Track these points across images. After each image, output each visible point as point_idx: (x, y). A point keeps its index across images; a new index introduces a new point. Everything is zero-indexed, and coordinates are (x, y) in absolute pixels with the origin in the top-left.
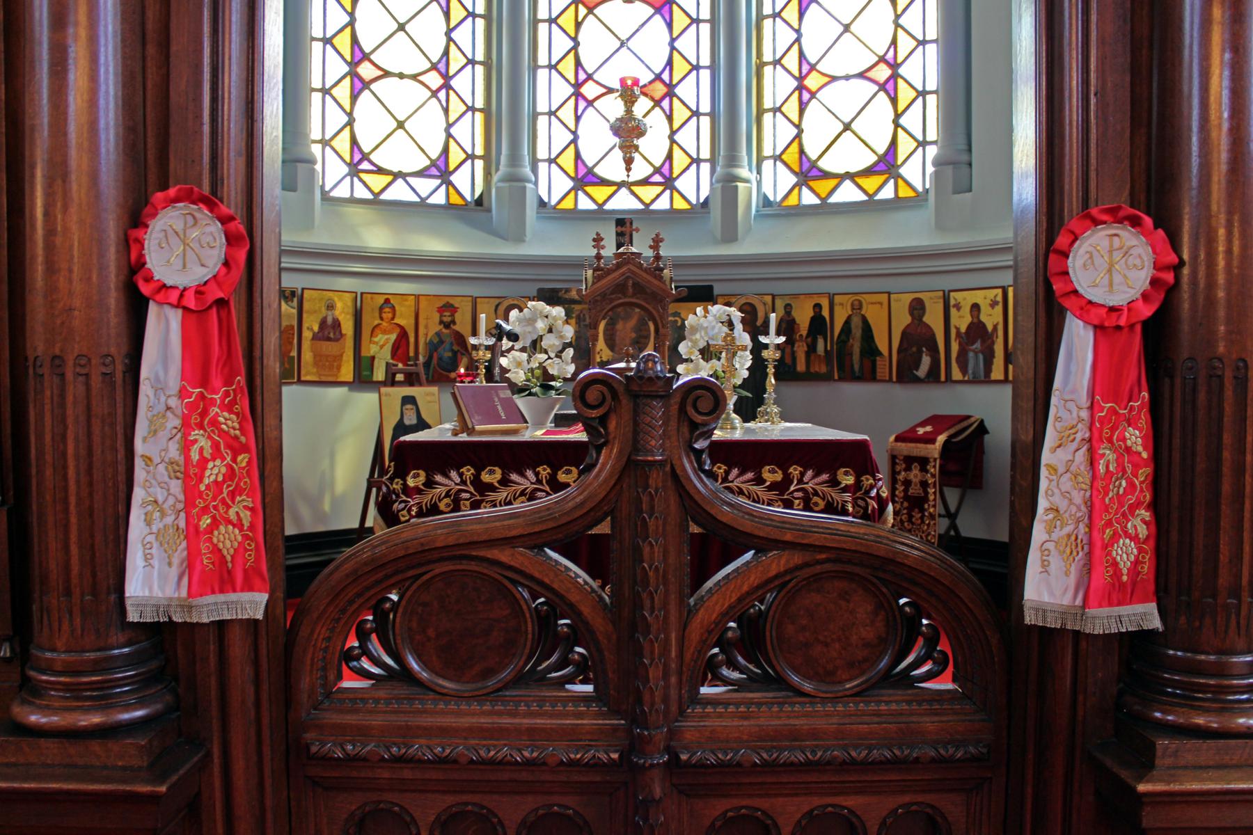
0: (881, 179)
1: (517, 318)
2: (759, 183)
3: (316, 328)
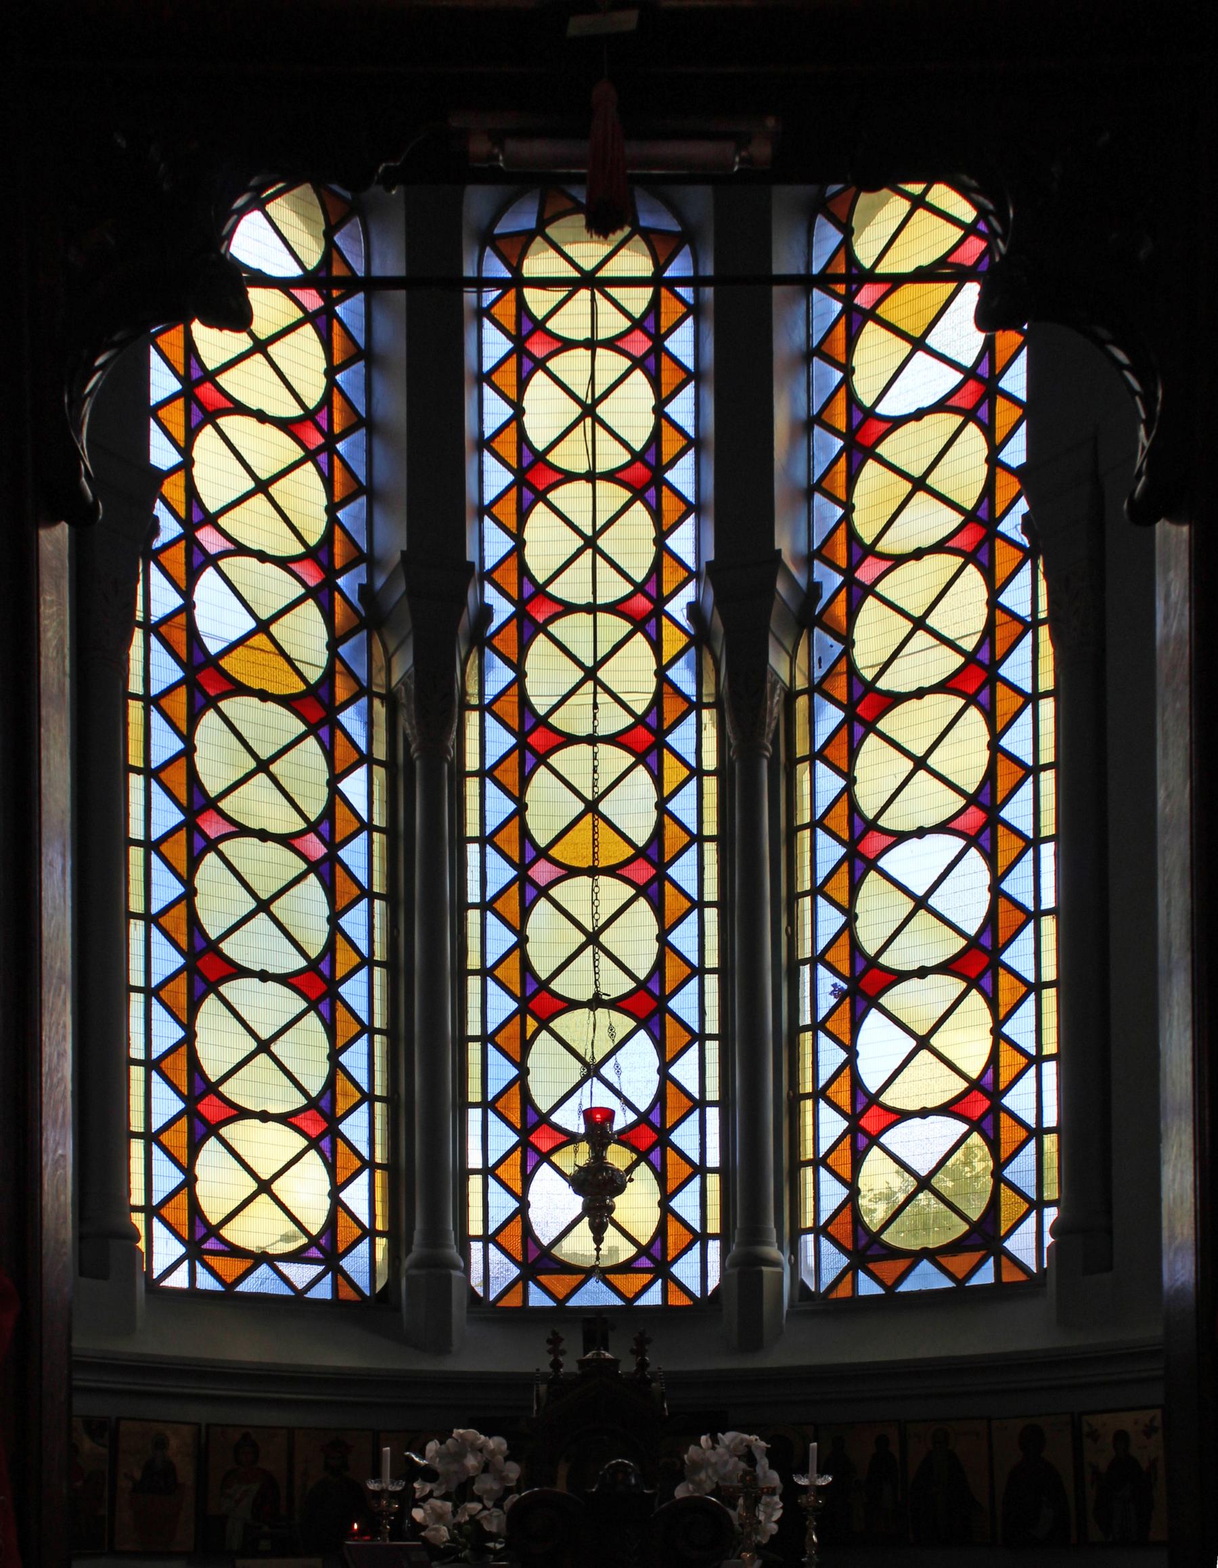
0: (975, 1257)
1: (437, 1452)
2: (795, 1267)
3: (138, 1475)
